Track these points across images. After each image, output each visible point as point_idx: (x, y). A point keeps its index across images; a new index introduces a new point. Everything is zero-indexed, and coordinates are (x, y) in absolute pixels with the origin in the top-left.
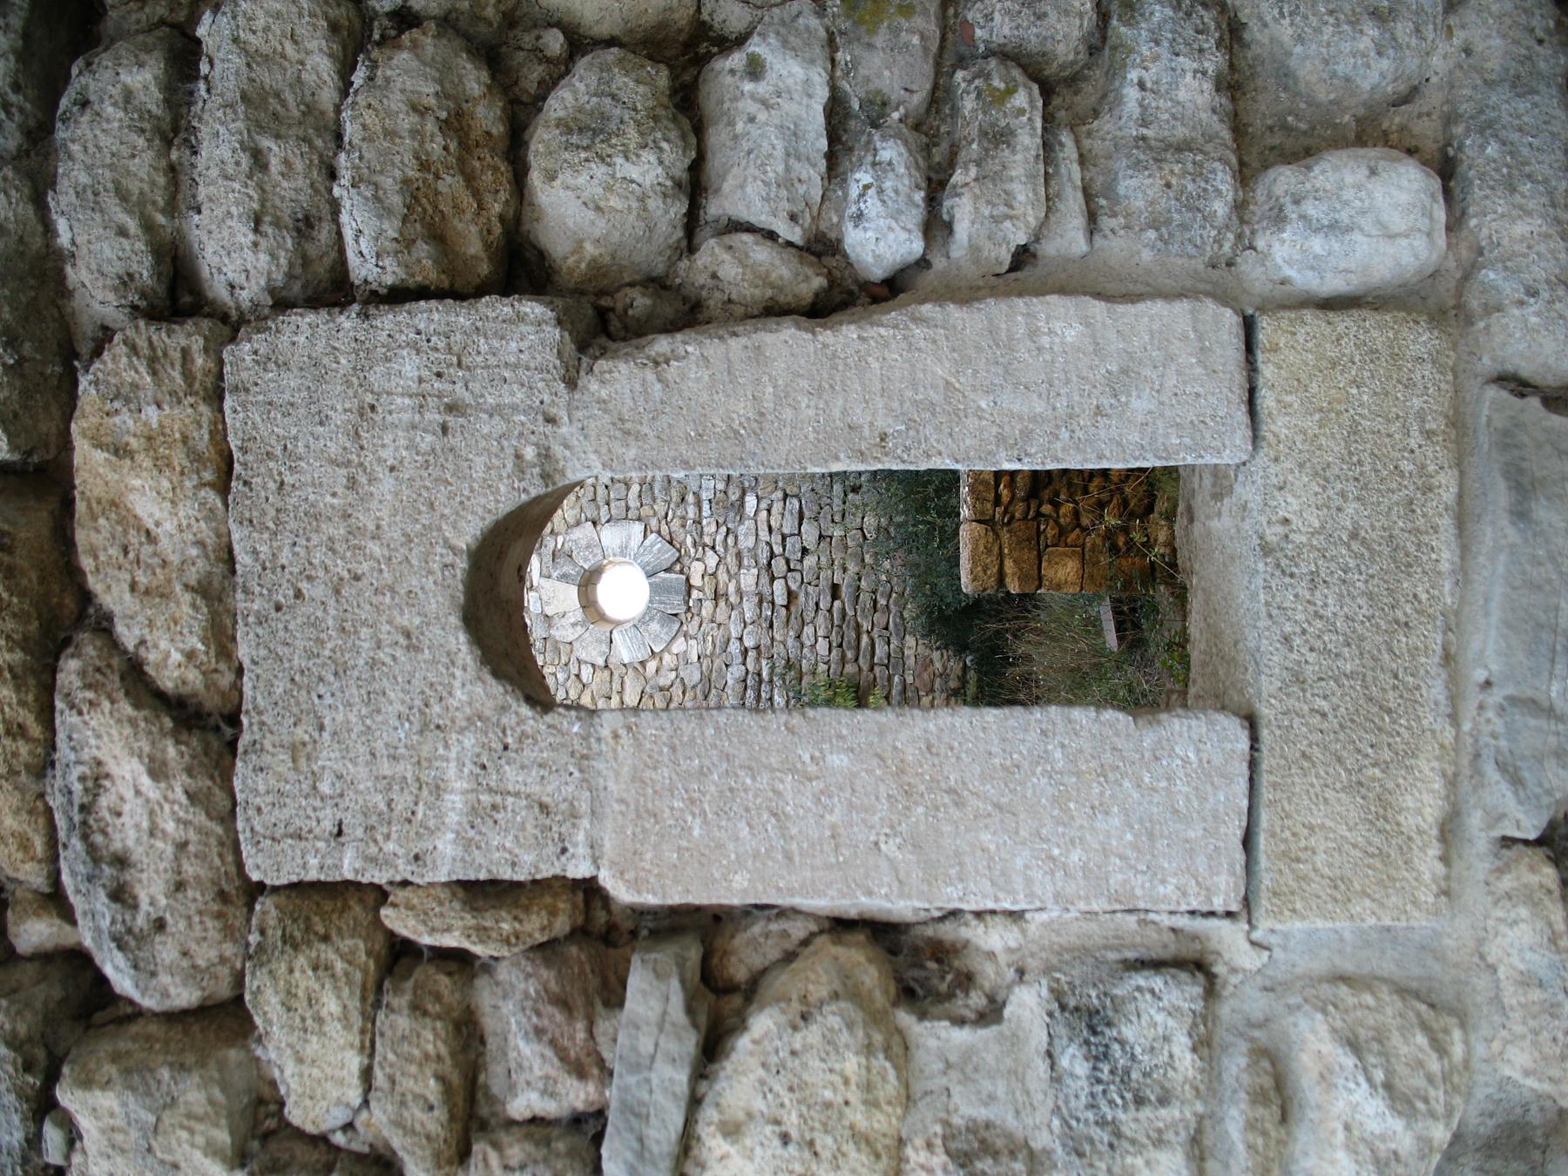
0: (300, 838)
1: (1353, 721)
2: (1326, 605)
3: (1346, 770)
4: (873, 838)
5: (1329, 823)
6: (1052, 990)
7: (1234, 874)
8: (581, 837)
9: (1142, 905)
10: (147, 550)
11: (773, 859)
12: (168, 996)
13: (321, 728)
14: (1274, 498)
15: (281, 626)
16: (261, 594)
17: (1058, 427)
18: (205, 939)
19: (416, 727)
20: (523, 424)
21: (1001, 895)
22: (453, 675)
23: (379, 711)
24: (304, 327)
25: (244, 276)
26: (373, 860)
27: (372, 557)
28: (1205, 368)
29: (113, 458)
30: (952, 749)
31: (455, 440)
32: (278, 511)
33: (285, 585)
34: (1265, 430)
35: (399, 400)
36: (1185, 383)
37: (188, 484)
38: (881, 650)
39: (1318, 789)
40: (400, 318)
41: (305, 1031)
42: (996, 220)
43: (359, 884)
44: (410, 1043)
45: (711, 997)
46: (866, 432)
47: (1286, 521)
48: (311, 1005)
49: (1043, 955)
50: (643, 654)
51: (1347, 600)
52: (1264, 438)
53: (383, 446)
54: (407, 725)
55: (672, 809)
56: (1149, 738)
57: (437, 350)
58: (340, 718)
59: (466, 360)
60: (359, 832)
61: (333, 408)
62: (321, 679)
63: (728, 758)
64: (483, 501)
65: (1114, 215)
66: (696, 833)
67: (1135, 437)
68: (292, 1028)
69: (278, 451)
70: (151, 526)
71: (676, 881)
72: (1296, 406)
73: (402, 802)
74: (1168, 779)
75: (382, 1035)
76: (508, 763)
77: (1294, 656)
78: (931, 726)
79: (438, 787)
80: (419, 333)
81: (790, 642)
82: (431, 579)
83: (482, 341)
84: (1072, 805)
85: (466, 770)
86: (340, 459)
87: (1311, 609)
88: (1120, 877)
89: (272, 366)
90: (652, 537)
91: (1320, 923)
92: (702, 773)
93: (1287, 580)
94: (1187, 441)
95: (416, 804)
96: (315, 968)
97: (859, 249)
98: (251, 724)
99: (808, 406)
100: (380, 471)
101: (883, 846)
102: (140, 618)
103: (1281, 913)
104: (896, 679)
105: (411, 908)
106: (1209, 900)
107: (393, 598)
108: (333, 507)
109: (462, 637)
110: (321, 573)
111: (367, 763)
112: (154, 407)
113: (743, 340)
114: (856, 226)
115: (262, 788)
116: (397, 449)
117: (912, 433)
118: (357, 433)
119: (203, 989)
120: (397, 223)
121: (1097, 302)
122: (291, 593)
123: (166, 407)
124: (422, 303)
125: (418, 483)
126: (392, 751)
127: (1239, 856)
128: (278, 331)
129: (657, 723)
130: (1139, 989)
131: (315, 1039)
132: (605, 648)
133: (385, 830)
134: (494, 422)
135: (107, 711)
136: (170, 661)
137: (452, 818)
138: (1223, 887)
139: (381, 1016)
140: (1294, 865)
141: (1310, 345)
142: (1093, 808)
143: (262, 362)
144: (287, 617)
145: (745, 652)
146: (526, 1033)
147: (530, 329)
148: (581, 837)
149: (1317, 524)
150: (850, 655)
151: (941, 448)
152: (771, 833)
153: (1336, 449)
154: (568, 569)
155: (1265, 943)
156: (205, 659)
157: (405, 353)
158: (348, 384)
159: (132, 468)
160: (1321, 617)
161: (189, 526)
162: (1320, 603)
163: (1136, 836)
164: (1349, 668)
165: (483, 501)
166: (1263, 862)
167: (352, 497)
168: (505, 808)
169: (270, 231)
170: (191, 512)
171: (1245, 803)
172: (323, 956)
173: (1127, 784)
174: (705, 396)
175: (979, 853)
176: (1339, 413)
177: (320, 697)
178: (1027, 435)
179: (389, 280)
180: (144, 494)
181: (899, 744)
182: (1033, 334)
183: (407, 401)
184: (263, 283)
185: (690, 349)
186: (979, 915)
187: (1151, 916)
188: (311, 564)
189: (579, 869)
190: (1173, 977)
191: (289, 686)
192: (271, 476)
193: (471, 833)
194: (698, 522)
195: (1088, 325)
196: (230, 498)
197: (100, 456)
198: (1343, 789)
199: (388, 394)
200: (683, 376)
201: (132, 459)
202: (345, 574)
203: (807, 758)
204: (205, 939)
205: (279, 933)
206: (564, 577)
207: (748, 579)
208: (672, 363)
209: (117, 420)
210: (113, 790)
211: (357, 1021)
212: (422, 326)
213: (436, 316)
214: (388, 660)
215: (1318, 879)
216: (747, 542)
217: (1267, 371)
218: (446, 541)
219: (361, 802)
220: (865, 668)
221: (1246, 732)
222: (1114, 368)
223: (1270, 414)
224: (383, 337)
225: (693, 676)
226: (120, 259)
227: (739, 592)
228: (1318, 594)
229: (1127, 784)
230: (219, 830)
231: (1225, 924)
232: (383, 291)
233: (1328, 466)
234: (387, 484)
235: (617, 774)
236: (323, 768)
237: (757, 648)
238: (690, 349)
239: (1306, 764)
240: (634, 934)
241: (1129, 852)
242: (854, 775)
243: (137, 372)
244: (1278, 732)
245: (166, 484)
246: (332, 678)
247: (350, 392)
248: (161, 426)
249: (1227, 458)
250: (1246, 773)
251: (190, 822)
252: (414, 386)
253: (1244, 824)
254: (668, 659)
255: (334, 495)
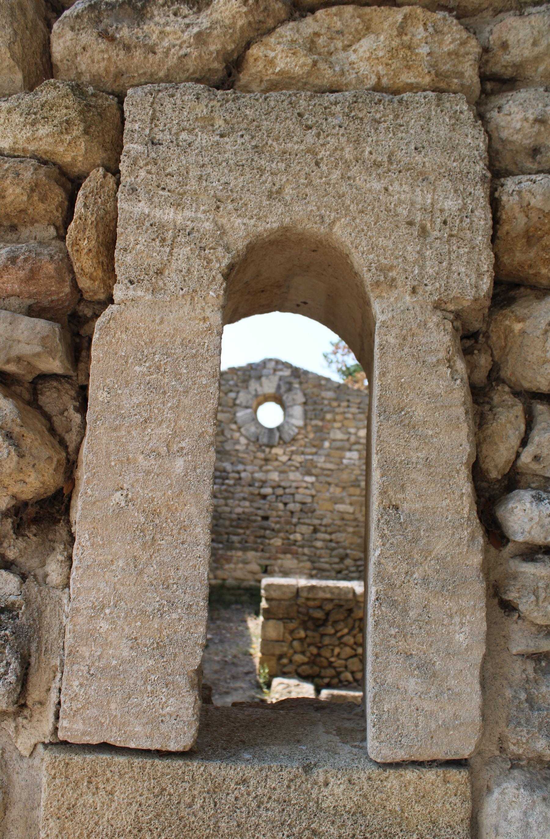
0: (152, 120)
1: (184, 827)
2: (267, 810)
3: (151, 819)
4: (125, 486)
5: (114, 805)
6: (13, 604)
7: (83, 734)
8: (140, 293)
9: (66, 669)
10: (339, 45)
11: (115, 419)
12: (59, 38)
13: (222, 136)
14: (343, 775)
15: (288, 115)
16: (309, 106)
17: (398, 627)
18: (93, 62)
19: (219, 194)
20: (412, 272)
21: (81, 571)
22: (252, 217)
23: (230, 171)
24: (477, 142)
25: (506, 112)
26: (135, 163)
27: (330, 173)
28: (435, 731)
29: (398, 24)
30: (183, 543)
31: (403, 230)
32: (362, 119)
33: (314, 120)
34: (391, 771)
35: (429, 196)
36: (425, 716)
37: (380, 68)
38: (235, 538)
39: (139, 798)
40: (481, 200)
41: (28, 114)
42: (535, 592)
43: (120, 154)
44: (14, 178)
45: (30, 378)
46: (399, 496)
47: (326, 784)
48: (43, 118)
49: (39, 599)
50: (239, 421)
51: (270, 826)
52: (385, 771)
53: (401, 185)
54: (221, 187)
55: (154, 354)
56: (182, 681)
57: (461, 221)
58: (228, 147)
59: (454, 240)
60: (153, 155)
61: (425, 155)
62: (253, 137)
63: (186, 392)
64: (364, 244)
65: (535, 671)
66: (137, 368)
67: (389, 680)
68: (30, 107)
69: (400, 121)
70: (354, 48)
71: (106, 353)
72: (406, 794)
73: (171, 182)
74: (152, 692)
75: (21, 162)
76: (191, 250)
77: (233, 785)
78: (199, 530)
79: (179, 205)
80: (472, 211)
81: (242, 495)
82: (314, 208)
83: (466, 250)
84: (139, 624)
85: (189, 223)
86: (393, 158)
87: (266, 799)
88: (87, 654)
89: (453, 121)
90: (296, 430)
91: (44, 796)
92: (177, 376)
93: (286, 782)
94: (385, 716)
95: (169, 191)
96: (67, 121)
97: (517, 498)
98: (227, 94)
99: (418, 458)
100: (384, 182)
101: (119, 493)
102: (297, 36)
103: (54, 768)
104: (221, 546)
105: (102, 186)
106: (67, 716)
107: (303, 184)
108: (363, 152)
109: (275, 225)
110: (321, 141)
111: (197, 162)
112: (429, 51)
113: (463, 417)
114: (533, 497)
115: (186, 98)
116: (399, 193)
117: (398, 527)
118: (409, 169)
119: (62, 61)
120: (539, 205)
121: (481, 656)
122: (309, 123)
123: (428, 58)
124: (491, 215)
125: (376, 204)
126: (205, 177)
127: (95, 741)
128: (474, 127)
129: (212, 347)
130: (8, 664)
131: (22, 120)
132: (244, 404)
133: (153, 171)
134: (414, 253)
135: (241, 9)
136: (269, 52)
137: (158, 213)
138: (75, 726)
139: (33, 162)
140: (86, 779)
141: (448, 806)
142: (136, 639)
143: (456, 116)
144: (294, 120)
145: (238, 472)
146: (14, 252)
147: (473, 281)
148: (140, 293)
149: (324, 805)
150: (234, 523)
151: (388, 545)
152: (133, 418)
153: (375, 821)
154: (283, 389)
155: (35, 754)
156: (269, 72)
157: (460, 201)
158: (441, 166)
159: (391, 36)
160: (259, 807)
161: (354, 69)
162: (269, 806)
163: (115, 667)
164: (223, 825)
165: (364, 244)
166: (89, 757)
167: (369, 164)
168: (163, 246)
169: (535, 129)
170: (362, 69)
171: (132, 745)
172: (76, 128)
173: (151, 662)
174: (426, 389)
175: (110, 558)
176: (400, 824)
177: (242, 136)
178: (394, 604)
179: (504, 198)
180: (374, 42)
181: (188, 507)
182: (461, 612)
183: (429, 201)
184: (502, 124)
185: (458, 382)
186: (70, 558)
187: (59, 675)
188: (327, 136)
189: (118, 293)
190: (15, 690)
191: (250, 118)
192: (384, 116)
193: (147, 224)
194: (303, 453)
195: (466, 650)
196: (371, 92)
197: (399, 18)
198: (137, 817)
199: (434, 190)
200: (440, 377)
201: (397, 36)
202: (319, 157)
203: (183, 444)
204: (93, 62)
205: (92, 104)
206: (279, 387)
207: (275, 476)
208: (450, 370)
209: (421, 29)
210: (191, 12)
211: (32, 147)
212: (476, 213)
213: (482, 223)
214: (264, 178)
215: (75, 795)
216: (292, 476)
217: (430, 775)
218: (339, 219)
219: (173, 157)
220: (228, 530)
221: (181, 749)
222: (437, 667)
223: (401, 776)
224: (470, 189)
225: (228, 447)
226: (518, 41)
227: (267, 471)
228: (275, 804)
229: (151, 662)
230: (161, 74)
231: (49, 727)
232: (497, 195)
233: (364, 816)
234: (377, 186)
235: (180, 319)
236: (196, 135)
237: (240, 479)
238: (458, 382)
239: (156, 791)
240: (78, 335)
241: (104, 661)
242: (169, 477)
243: (451, 43)
244: (180, 772)
245: (381, 54)
246: (253, 144)
247: (435, 167)
248: (416, 55)
249: (371, 743)
250: (153, 748)
251: (167, 57)
252: (439, 206)
253: (118, 744)
254: (237, 435)
255: (371, 153)
